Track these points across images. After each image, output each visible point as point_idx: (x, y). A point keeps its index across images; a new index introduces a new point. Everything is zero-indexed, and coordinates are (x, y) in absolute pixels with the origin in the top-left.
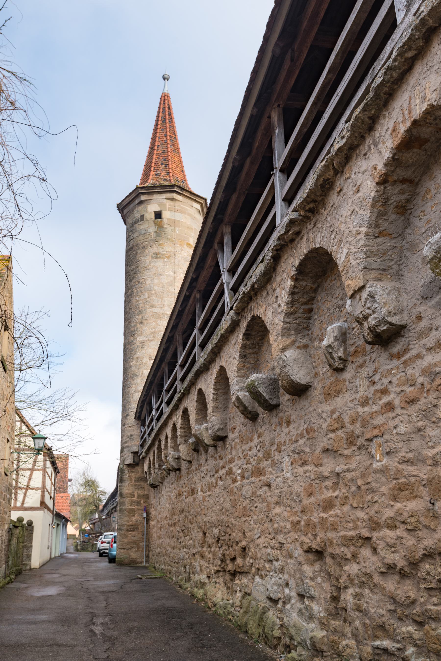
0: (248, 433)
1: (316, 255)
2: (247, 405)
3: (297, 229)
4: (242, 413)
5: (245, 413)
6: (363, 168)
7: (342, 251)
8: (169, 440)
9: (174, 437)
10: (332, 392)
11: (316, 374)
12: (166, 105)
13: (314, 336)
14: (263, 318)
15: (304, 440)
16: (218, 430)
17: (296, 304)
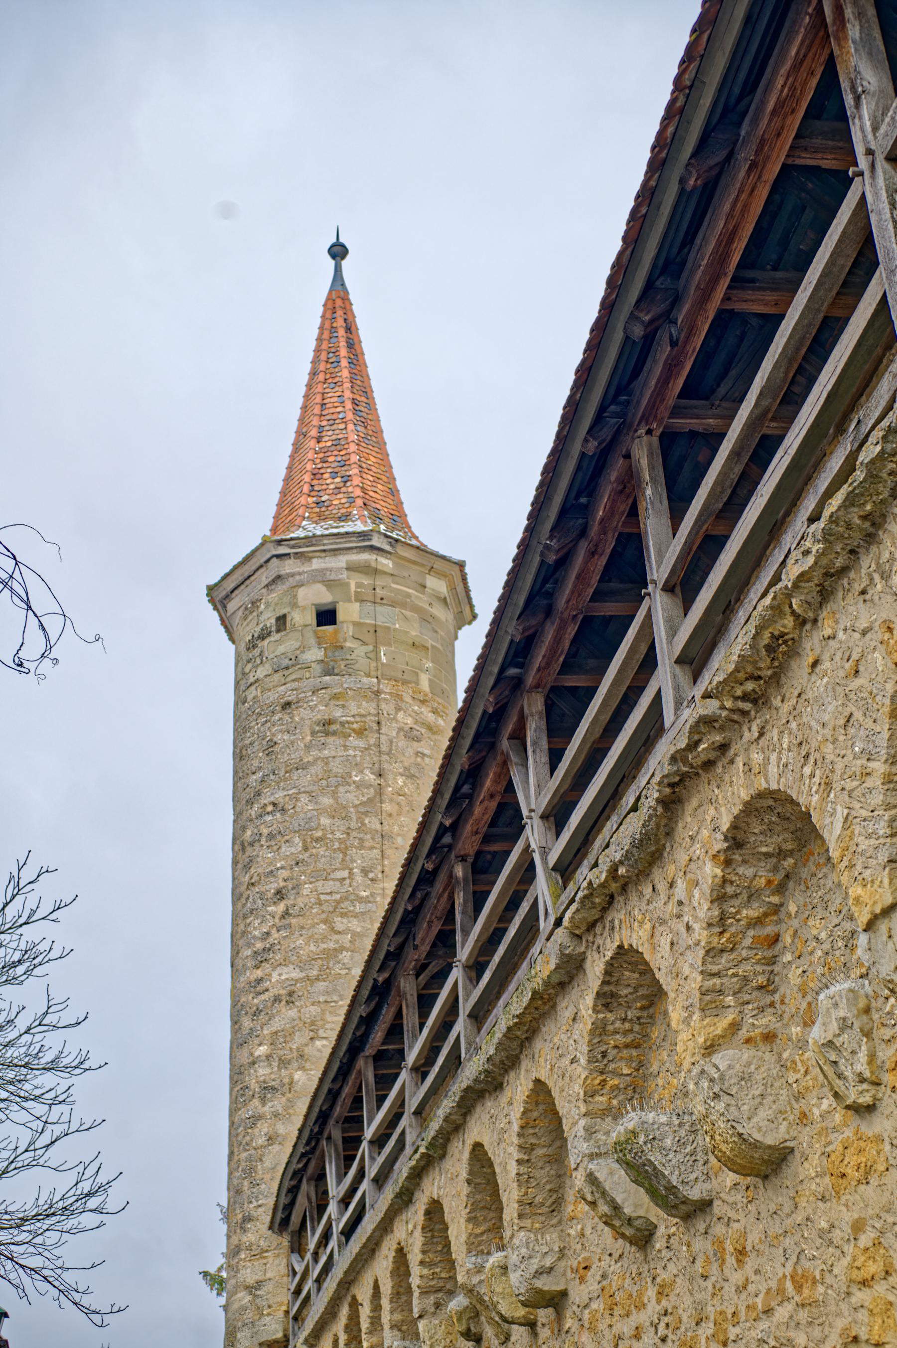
0: (628, 1281)
1: (771, 802)
2: (619, 1200)
3: (718, 738)
4: (606, 1223)
5: (617, 1223)
6: (863, 624)
7: (834, 809)
8: (385, 1302)
9: (402, 1291)
10: (849, 1171)
11: (804, 1115)
12: (340, 323)
13: (790, 1009)
14: (647, 957)
15: (789, 1307)
16: (538, 1273)
17: (731, 924)
